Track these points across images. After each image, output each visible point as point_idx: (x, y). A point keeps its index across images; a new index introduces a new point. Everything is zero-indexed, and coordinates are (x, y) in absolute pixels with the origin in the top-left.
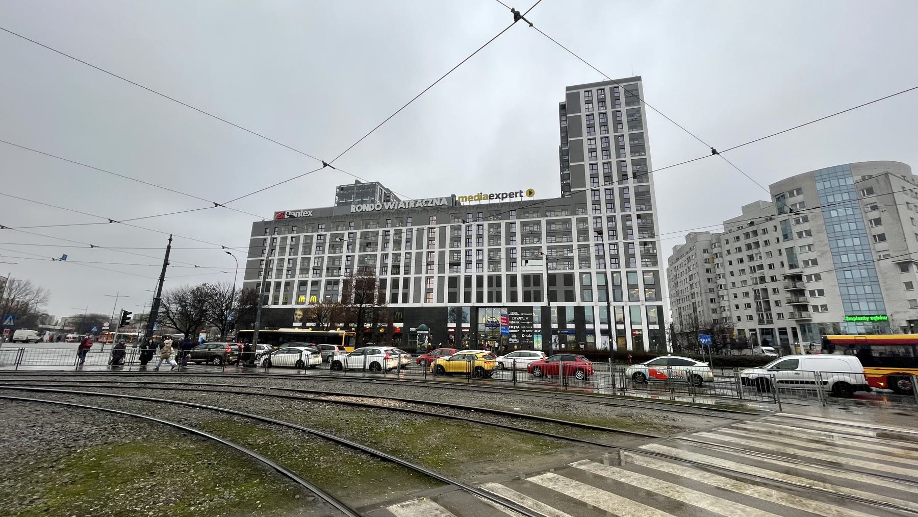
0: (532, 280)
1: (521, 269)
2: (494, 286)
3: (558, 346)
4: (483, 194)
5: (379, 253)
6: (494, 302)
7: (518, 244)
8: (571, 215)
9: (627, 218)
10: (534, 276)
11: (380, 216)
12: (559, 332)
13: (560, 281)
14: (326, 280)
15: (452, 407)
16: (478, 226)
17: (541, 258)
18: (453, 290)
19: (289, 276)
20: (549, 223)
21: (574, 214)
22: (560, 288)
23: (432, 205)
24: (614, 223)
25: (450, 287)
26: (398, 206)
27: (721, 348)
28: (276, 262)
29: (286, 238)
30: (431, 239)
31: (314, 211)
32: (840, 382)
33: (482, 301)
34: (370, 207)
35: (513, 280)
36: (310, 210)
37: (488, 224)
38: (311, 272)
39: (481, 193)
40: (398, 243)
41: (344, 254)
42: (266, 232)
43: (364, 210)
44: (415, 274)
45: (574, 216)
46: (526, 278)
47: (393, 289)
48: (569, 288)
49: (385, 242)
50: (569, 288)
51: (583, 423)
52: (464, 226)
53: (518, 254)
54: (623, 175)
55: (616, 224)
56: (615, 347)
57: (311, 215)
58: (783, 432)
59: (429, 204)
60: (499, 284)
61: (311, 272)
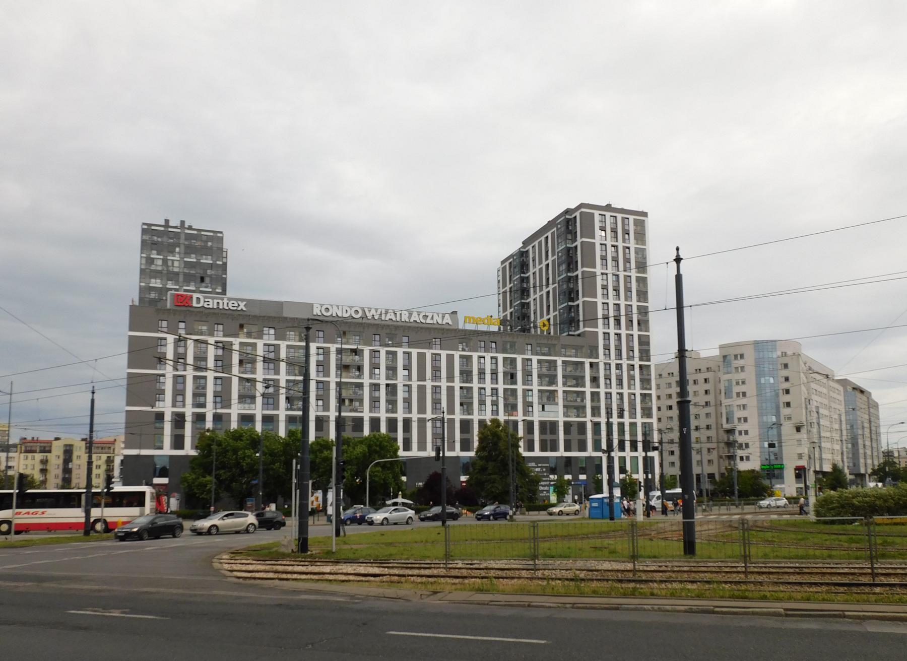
1: (537, 417)
2: (368, 419)
4: (493, 318)
5: (366, 380)
6: (316, 434)
7: (535, 387)
8: (365, 344)
9: (632, 367)
11: (364, 328)
12: (573, 483)
13: (574, 430)
16: (480, 357)
18: (466, 436)
19: (219, 405)
20: (340, 351)
21: (260, 337)
22: (575, 436)
23: (431, 322)
25: (461, 432)
26: (386, 317)
30: (436, 369)
31: (249, 302)
34: (344, 311)
36: (242, 300)
37: (418, 353)
38: (259, 400)
39: (491, 316)
40: (392, 370)
45: (284, 342)
46: (543, 424)
48: (582, 437)
49: (375, 366)
50: (582, 437)
52: (171, 338)
53: (535, 399)
55: (622, 372)
56: (541, 488)
57: (244, 309)
59: (429, 321)
61: (259, 400)
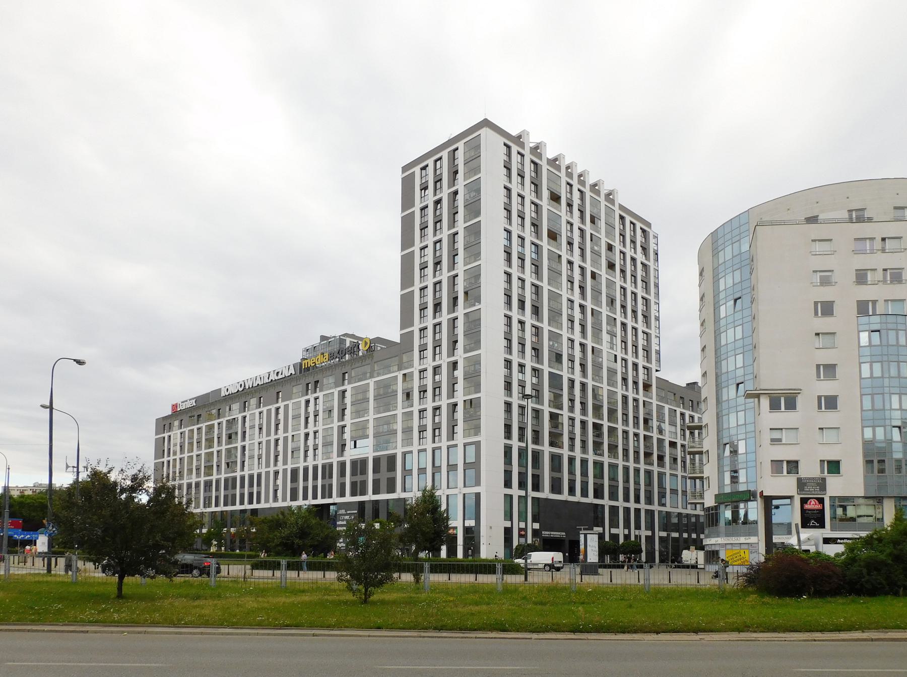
0: (359, 466)
3: (742, 513)
10: (360, 461)
14: (249, 474)
15: (676, 640)
17: (367, 437)
24: (509, 370)
25: (291, 482)
27: (381, 545)
28: (400, 419)
29: (213, 425)
32: (514, 574)
33: (330, 496)
35: (342, 465)
36: (193, 399)
41: (399, 412)
42: (278, 398)
43: (230, 393)
44: (338, 457)
47: (352, 476)
51: (70, 662)
54: (895, 208)
58: (816, 639)
60: (364, 471)
